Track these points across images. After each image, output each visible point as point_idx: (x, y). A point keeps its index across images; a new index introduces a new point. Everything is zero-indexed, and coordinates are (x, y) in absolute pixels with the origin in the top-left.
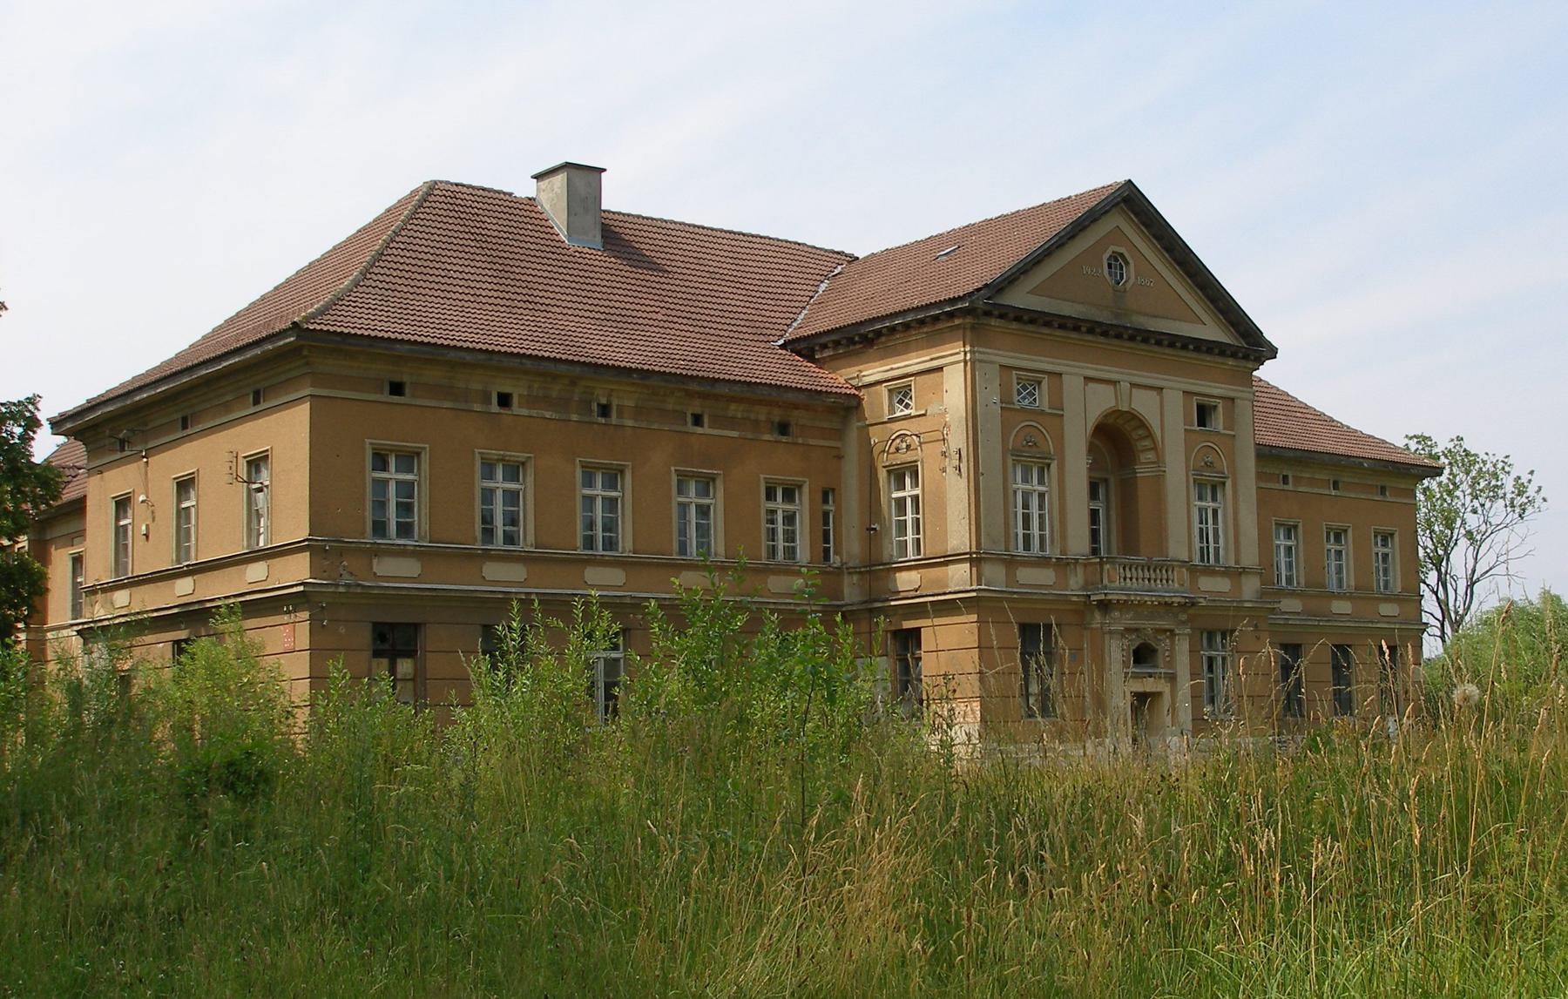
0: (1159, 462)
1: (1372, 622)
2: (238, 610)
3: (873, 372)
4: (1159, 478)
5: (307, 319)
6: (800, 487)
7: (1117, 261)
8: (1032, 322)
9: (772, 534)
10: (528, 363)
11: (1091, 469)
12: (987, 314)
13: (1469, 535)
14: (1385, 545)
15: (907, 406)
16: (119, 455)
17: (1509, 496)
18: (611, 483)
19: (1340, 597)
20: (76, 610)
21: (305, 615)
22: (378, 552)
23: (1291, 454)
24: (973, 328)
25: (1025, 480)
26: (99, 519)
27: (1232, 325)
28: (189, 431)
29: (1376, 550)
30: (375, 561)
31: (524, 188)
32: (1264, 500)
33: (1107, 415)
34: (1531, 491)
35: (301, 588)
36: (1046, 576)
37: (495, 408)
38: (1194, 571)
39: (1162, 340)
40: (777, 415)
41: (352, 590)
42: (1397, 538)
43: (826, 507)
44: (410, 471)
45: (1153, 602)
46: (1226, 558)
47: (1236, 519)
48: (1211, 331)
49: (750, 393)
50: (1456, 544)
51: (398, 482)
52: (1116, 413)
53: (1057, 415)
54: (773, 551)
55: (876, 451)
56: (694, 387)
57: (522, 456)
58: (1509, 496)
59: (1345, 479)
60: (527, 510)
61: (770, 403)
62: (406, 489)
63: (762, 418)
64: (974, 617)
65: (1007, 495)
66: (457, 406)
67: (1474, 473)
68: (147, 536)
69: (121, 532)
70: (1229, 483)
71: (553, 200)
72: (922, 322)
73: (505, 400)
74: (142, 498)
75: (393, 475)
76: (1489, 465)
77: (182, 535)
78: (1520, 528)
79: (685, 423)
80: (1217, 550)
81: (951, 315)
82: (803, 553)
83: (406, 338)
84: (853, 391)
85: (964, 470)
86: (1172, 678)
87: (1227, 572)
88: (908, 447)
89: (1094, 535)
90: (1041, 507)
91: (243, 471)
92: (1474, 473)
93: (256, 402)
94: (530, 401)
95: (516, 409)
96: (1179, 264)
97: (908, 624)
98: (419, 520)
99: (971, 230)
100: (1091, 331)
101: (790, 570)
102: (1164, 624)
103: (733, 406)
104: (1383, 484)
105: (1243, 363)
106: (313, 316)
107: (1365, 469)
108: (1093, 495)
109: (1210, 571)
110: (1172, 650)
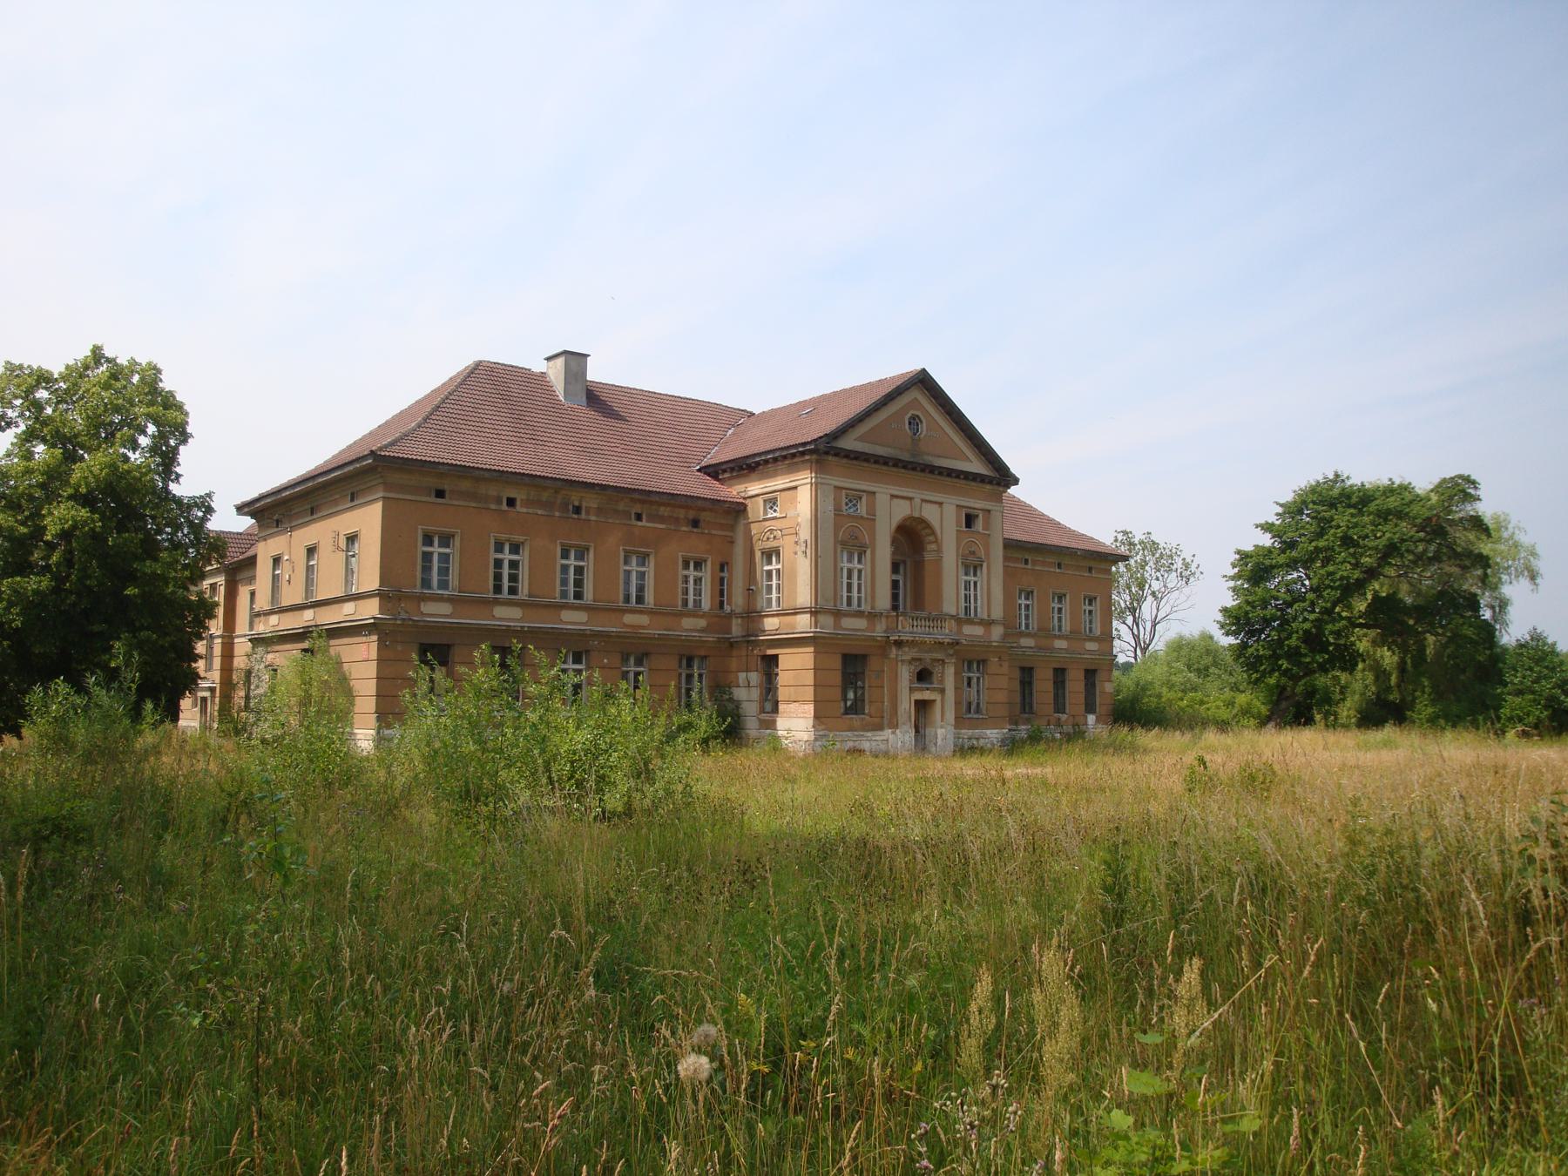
0: (939, 550)
2: (324, 634)
3: (755, 488)
4: (938, 562)
5: (381, 449)
6: (705, 561)
7: (916, 420)
8: (856, 458)
9: (686, 592)
10: (526, 479)
11: (894, 553)
12: (827, 453)
13: (1153, 594)
14: (1090, 604)
15: (775, 511)
16: (276, 530)
17: (1179, 571)
18: (580, 557)
19: (1060, 637)
20: (251, 627)
21: (375, 638)
22: (423, 598)
23: (1030, 546)
24: (817, 462)
25: (850, 560)
26: (263, 569)
27: (990, 462)
28: (315, 517)
30: (422, 604)
31: (538, 366)
32: (1008, 574)
33: (905, 520)
34: (1193, 568)
35: (372, 621)
36: (861, 623)
37: (504, 507)
38: (959, 621)
40: (692, 514)
41: (406, 623)
43: (722, 574)
44: (448, 546)
46: (982, 612)
47: (989, 589)
48: (976, 466)
49: (673, 500)
51: (440, 554)
52: (911, 518)
53: (871, 519)
54: (685, 602)
55: (755, 539)
56: (636, 496)
57: (521, 538)
58: (1179, 571)
60: (524, 573)
61: (687, 507)
62: (445, 558)
63: (682, 516)
64: (812, 649)
65: (837, 570)
66: (480, 505)
67: (1157, 555)
68: (289, 581)
69: (275, 578)
70: (985, 565)
71: (556, 374)
72: (785, 457)
73: (511, 502)
74: (286, 558)
75: (436, 549)
76: (1167, 551)
77: (309, 582)
78: (1186, 590)
79: (630, 519)
80: (976, 608)
81: (803, 453)
82: (706, 604)
83: (446, 461)
84: (741, 500)
85: (808, 553)
86: (942, 691)
87: (982, 622)
88: (775, 537)
89: (895, 597)
90: (859, 578)
91: (343, 543)
92: (1157, 555)
93: (352, 500)
94: (528, 503)
95: (519, 508)
96: (956, 423)
97: (770, 652)
98: (453, 578)
99: (824, 398)
100: (895, 465)
101: (694, 614)
102: (939, 656)
103: (662, 509)
105: (996, 487)
106: (386, 446)
108: (895, 568)
109: (970, 622)
110: (943, 673)
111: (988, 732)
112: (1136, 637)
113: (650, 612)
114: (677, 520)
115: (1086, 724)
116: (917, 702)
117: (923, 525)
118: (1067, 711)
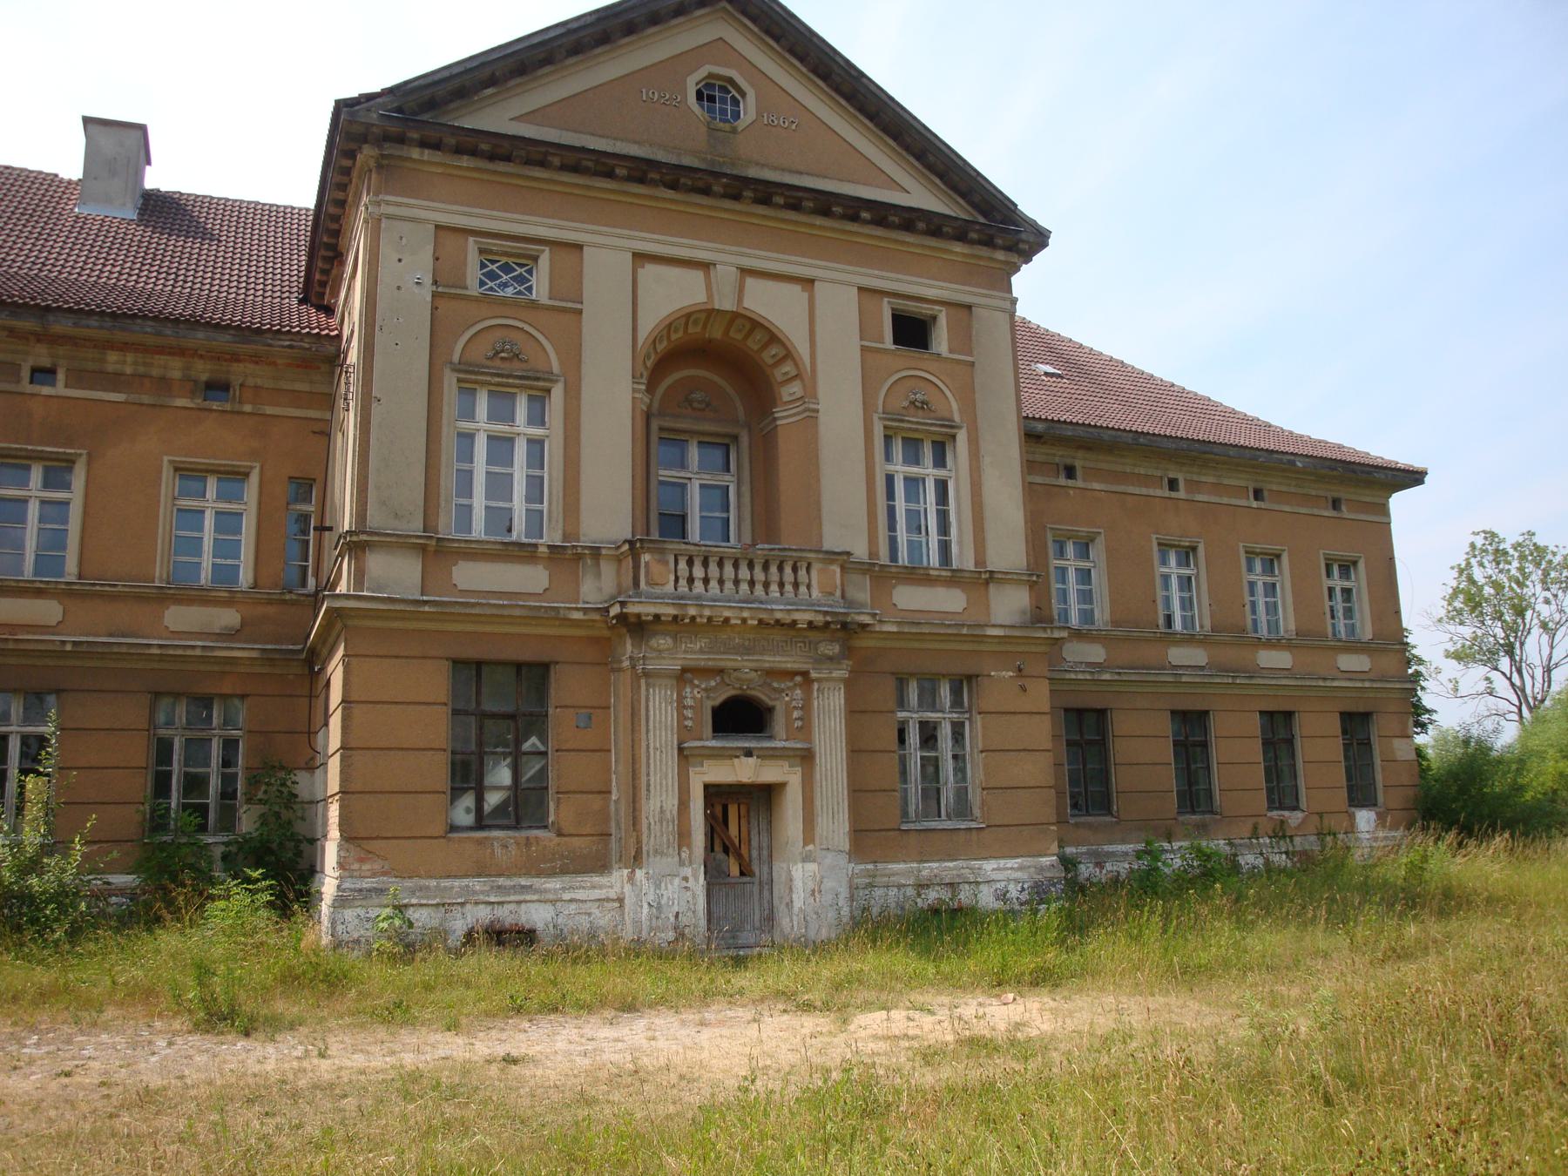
1: (1325, 679)
13: (1544, 625)
19: (1272, 644)
25: (502, 413)
29: (1327, 583)
39: (801, 199)
40: (203, 371)
42: (1361, 565)
45: (744, 620)
50: (1529, 633)
53: (568, 310)
59: (1275, 487)
86: (806, 758)
96: (848, 99)
103: (113, 357)
104: (1336, 495)
107: (1298, 471)
110: (806, 707)
111: (989, 866)
112: (1520, 691)
113: (68, 593)
114: (164, 385)
115: (1351, 829)
116: (716, 795)
117: (759, 335)
118: (1303, 804)
